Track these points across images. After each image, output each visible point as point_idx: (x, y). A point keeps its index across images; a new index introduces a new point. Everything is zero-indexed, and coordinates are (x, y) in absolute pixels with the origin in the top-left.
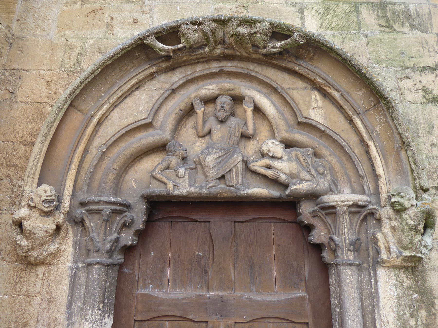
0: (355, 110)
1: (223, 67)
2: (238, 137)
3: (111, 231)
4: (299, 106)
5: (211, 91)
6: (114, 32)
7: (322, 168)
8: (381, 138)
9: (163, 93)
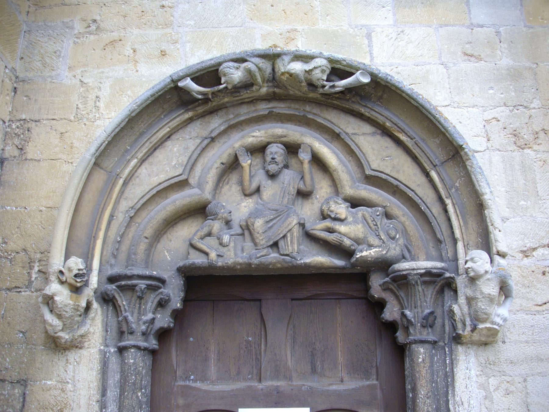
0: (431, 161)
1: (273, 108)
2: (293, 195)
3: (146, 311)
4: (367, 155)
5: (259, 139)
6: (138, 69)
7: (393, 231)
8: (462, 194)
9: (201, 143)
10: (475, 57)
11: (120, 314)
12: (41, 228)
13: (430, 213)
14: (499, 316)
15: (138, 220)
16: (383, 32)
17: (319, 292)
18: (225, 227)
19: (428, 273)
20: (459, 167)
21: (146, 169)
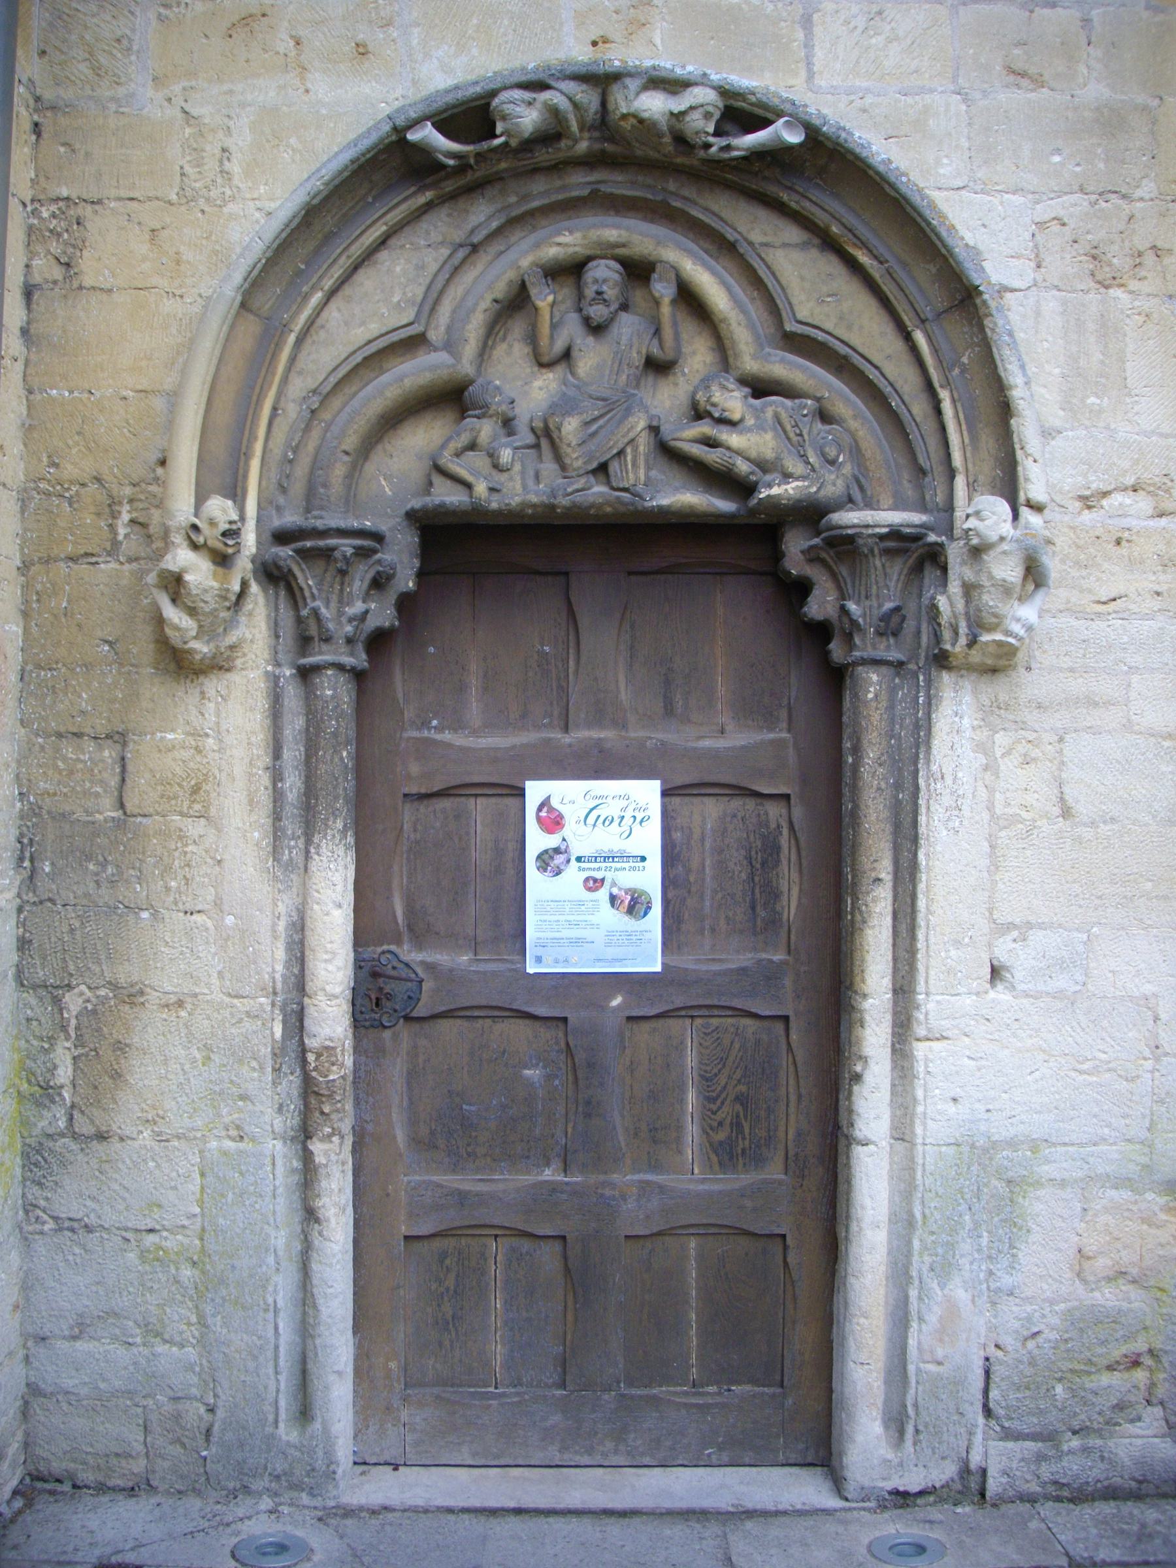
0: (915, 310)
2: (637, 368)
4: (789, 291)
5: (571, 250)
6: (309, 86)
9: (450, 256)
10: (1030, 78)
11: (300, 604)
12: (128, 434)
13: (907, 414)
14: (1018, 620)
15: (327, 416)
16: (837, 12)
17: (684, 561)
18: (502, 432)
19: (895, 534)
20: (970, 324)
21: (339, 310)
